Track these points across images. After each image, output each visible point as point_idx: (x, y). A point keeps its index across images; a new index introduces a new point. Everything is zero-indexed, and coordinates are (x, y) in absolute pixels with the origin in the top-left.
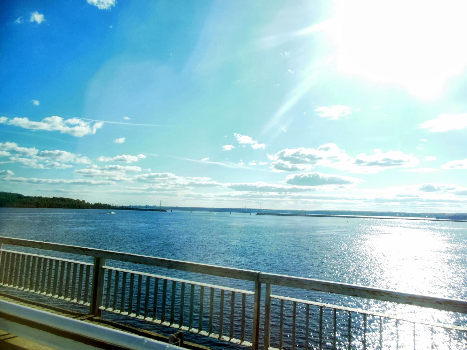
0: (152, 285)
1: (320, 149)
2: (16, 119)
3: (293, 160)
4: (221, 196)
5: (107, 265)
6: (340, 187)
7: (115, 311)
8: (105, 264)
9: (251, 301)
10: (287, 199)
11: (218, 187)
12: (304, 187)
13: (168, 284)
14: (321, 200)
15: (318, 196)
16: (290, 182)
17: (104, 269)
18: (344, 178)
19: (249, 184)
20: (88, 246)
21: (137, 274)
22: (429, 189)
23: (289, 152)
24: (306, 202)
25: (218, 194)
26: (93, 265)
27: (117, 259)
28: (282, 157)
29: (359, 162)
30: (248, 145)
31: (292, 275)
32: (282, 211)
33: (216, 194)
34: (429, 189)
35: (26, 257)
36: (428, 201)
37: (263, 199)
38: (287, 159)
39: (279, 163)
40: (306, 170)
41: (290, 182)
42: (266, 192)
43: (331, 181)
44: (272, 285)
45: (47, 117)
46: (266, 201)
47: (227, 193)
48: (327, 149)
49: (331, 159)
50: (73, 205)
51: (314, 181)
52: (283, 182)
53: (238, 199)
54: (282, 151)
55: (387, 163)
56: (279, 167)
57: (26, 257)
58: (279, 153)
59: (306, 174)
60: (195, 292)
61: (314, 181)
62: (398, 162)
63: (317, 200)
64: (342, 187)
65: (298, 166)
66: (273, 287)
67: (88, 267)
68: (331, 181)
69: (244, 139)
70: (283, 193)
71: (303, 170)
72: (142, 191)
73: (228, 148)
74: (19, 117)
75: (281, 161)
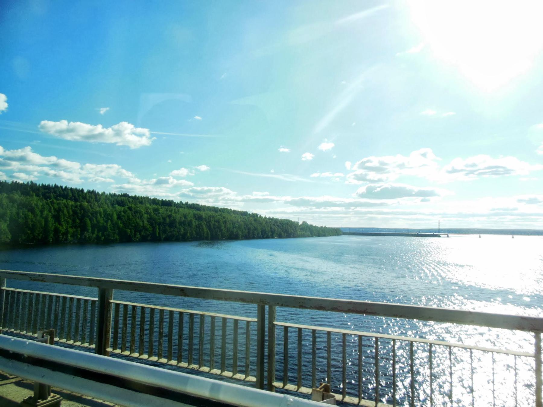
0: (166, 318)
2: (78, 123)
5: (114, 299)
6: (422, 201)
7: (170, 363)
8: (111, 297)
9: (254, 327)
11: (275, 202)
12: (378, 201)
13: (175, 315)
15: (390, 211)
16: (362, 196)
17: (3, 290)
19: (307, 198)
20: (219, 287)
21: (197, 314)
23: (375, 161)
24: (371, 219)
26: (97, 299)
27: (157, 293)
28: (362, 166)
29: (454, 171)
31: (108, 277)
32: (396, 230)
35: (47, 298)
39: (361, 174)
40: (390, 180)
41: (362, 196)
44: (256, 305)
45: (125, 121)
46: (325, 217)
48: (424, 155)
50: (232, 233)
54: (365, 159)
55: (495, 170)
56: (361, 178)
57: (47, 298)
60: (216, 324)
66: (279, 310)
67: (93, 302)
70: (352, 208)
72: (502, 211)
73: (308, 156)
74: (81, 122)
75: (363, 172)
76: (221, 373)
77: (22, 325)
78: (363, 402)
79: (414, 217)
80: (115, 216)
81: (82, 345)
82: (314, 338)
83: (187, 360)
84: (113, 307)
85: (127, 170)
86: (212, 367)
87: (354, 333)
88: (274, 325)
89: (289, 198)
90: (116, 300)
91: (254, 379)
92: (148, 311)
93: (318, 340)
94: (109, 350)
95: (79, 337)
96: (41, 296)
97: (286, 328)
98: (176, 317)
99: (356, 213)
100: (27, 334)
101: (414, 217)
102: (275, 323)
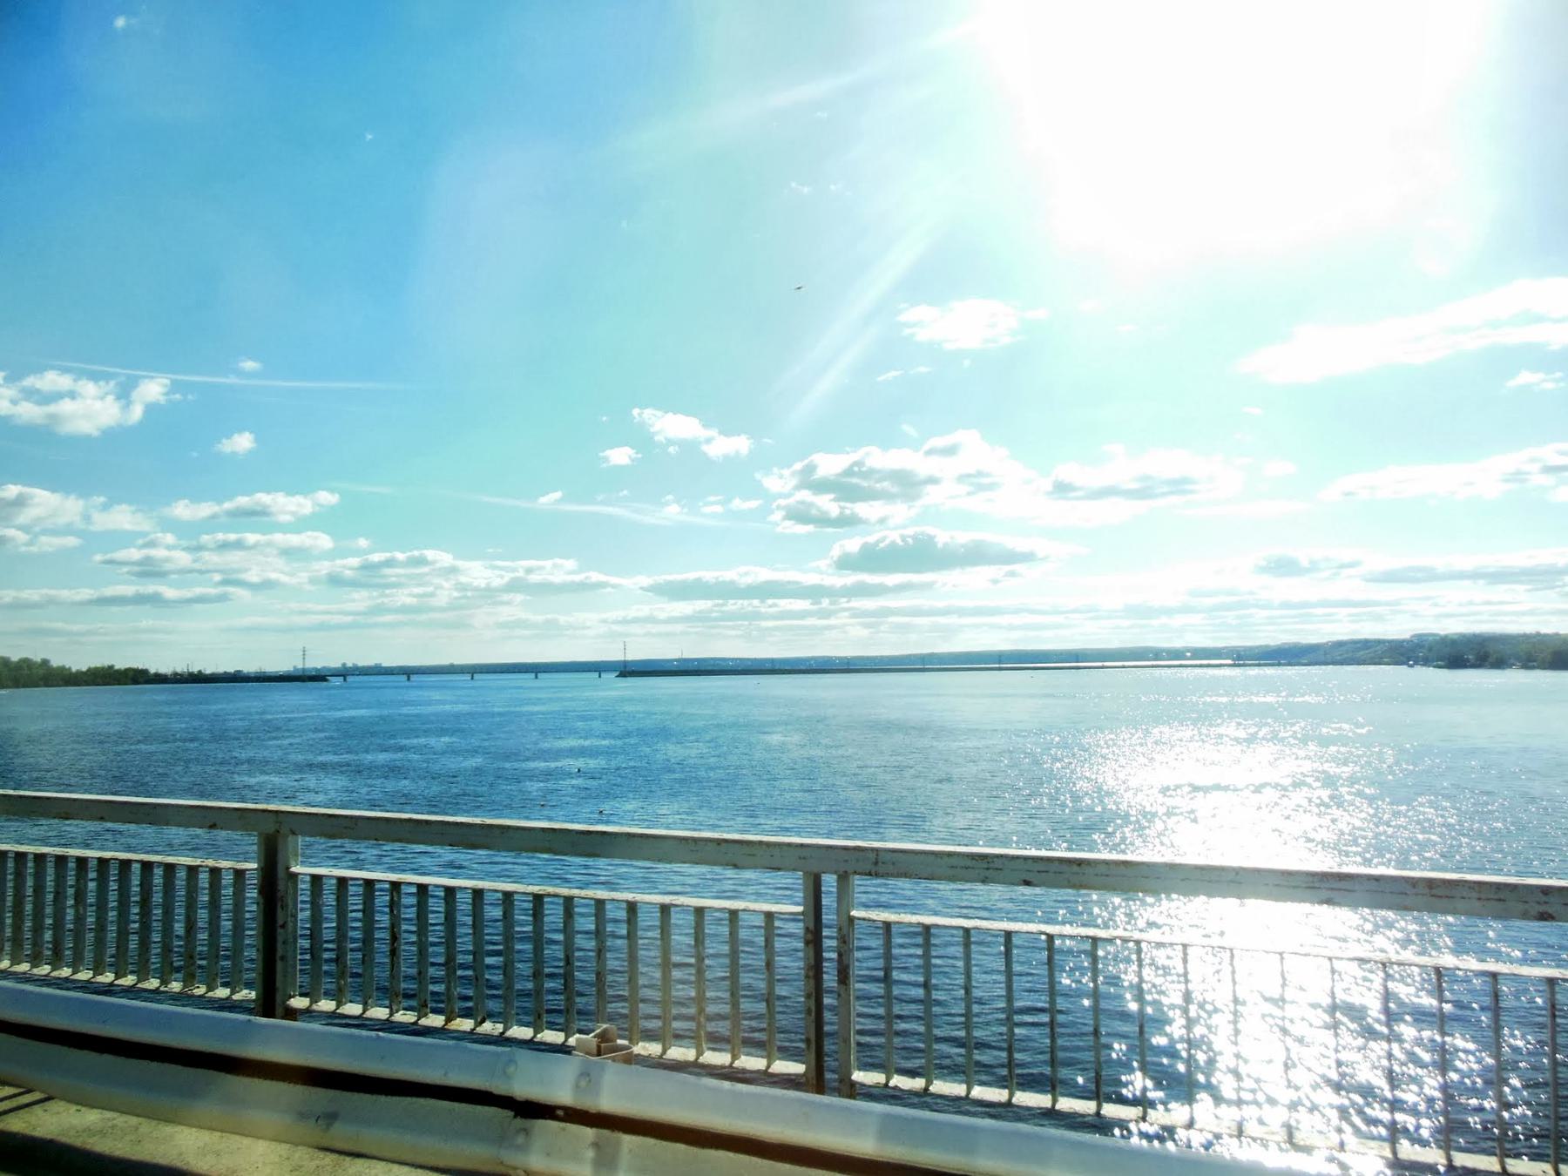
1: (930, 452)
3: (847, 487)
4: (625, 622)
10: (842, 619)
13: (352, 890)
14: (953, 620)
15: (940, 604)
16: (845, 563)
18: (1021, 545)
22: (1284, 567)
23: (829, 465)
25: (613, 615)
30: (690, 448)
33: (604, 616)
34: (1284, 567)
36: (1286, 605)
37: (765, 624)
38: (821, 487)
40: (889, 521)
42: (770, 602)
43: (975, 556)
46: (776, 628)
47: (645, 611)
49: (967, 481)
51: (920, 555)
52: (823, 564)
53: (679, 628)
58: (798, 466)
59: (894, 536)
61: (920, 555)
62: (1179, 486)
63: (942, 620)
64: (1012, 574)
65: (862, 509)
68: (975, 556)
69: (673, 426)
71: (882, 521)
73: (620, 456)
75: (805, 495)
76: (364, 1011)
77: (316, 975)
78: (1514, 1165)
79: (1017, 620)
80: (456, 594)
81: (210, 994)
82: (967, 944)
83: (355, 993)
84: (304, 886)
85: (291, 492)
86: (422, 1010)
87: (1067, 931)
88: (851, 920)
89: (646, 581)
90: (308, 865)
91: (797, 1068)
92: (330, 887)
93: (919, 952)
94: (299, 1003)
95: (327, 983)
96: (31, 857)
97: (700, 912)
98: (464, 903)
99: (857, 614)
100: (479, 1030)
101: (1017, 620)
102: (854, 913)
